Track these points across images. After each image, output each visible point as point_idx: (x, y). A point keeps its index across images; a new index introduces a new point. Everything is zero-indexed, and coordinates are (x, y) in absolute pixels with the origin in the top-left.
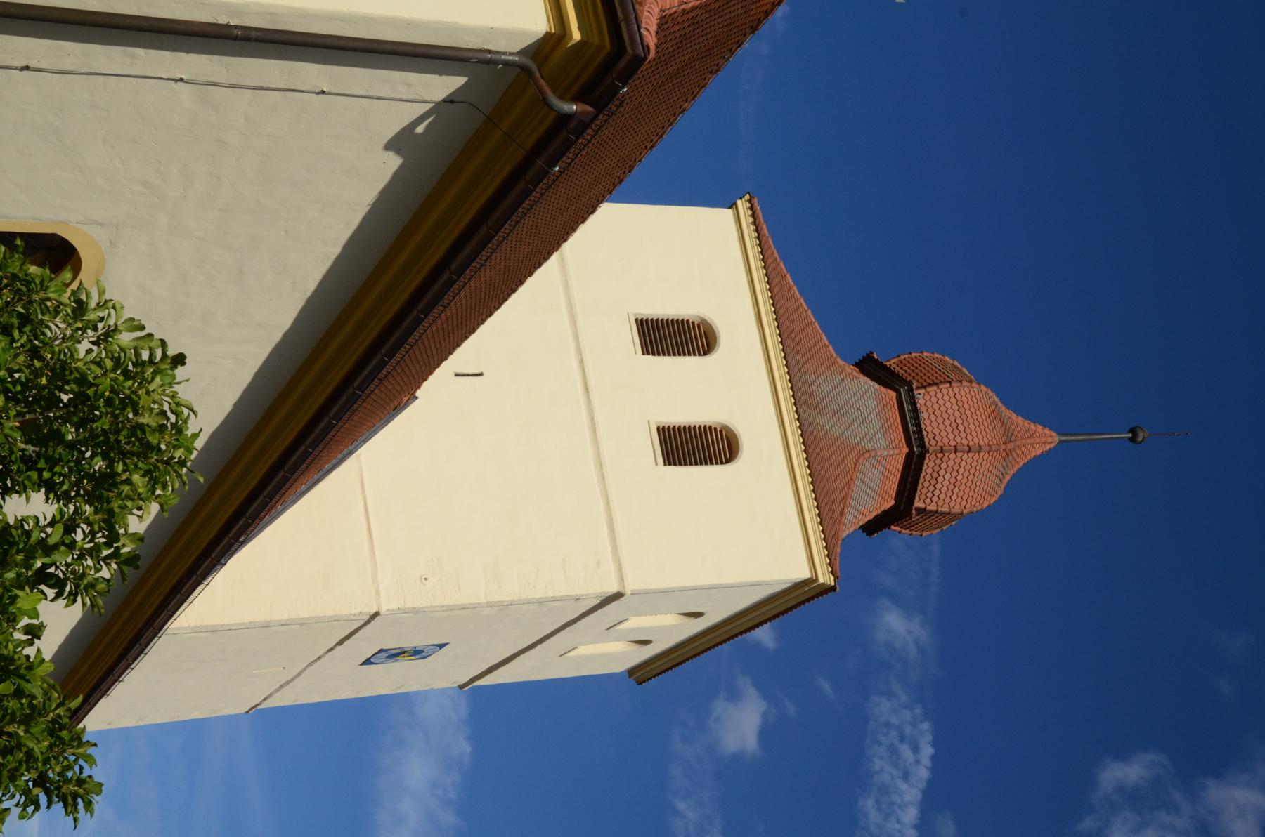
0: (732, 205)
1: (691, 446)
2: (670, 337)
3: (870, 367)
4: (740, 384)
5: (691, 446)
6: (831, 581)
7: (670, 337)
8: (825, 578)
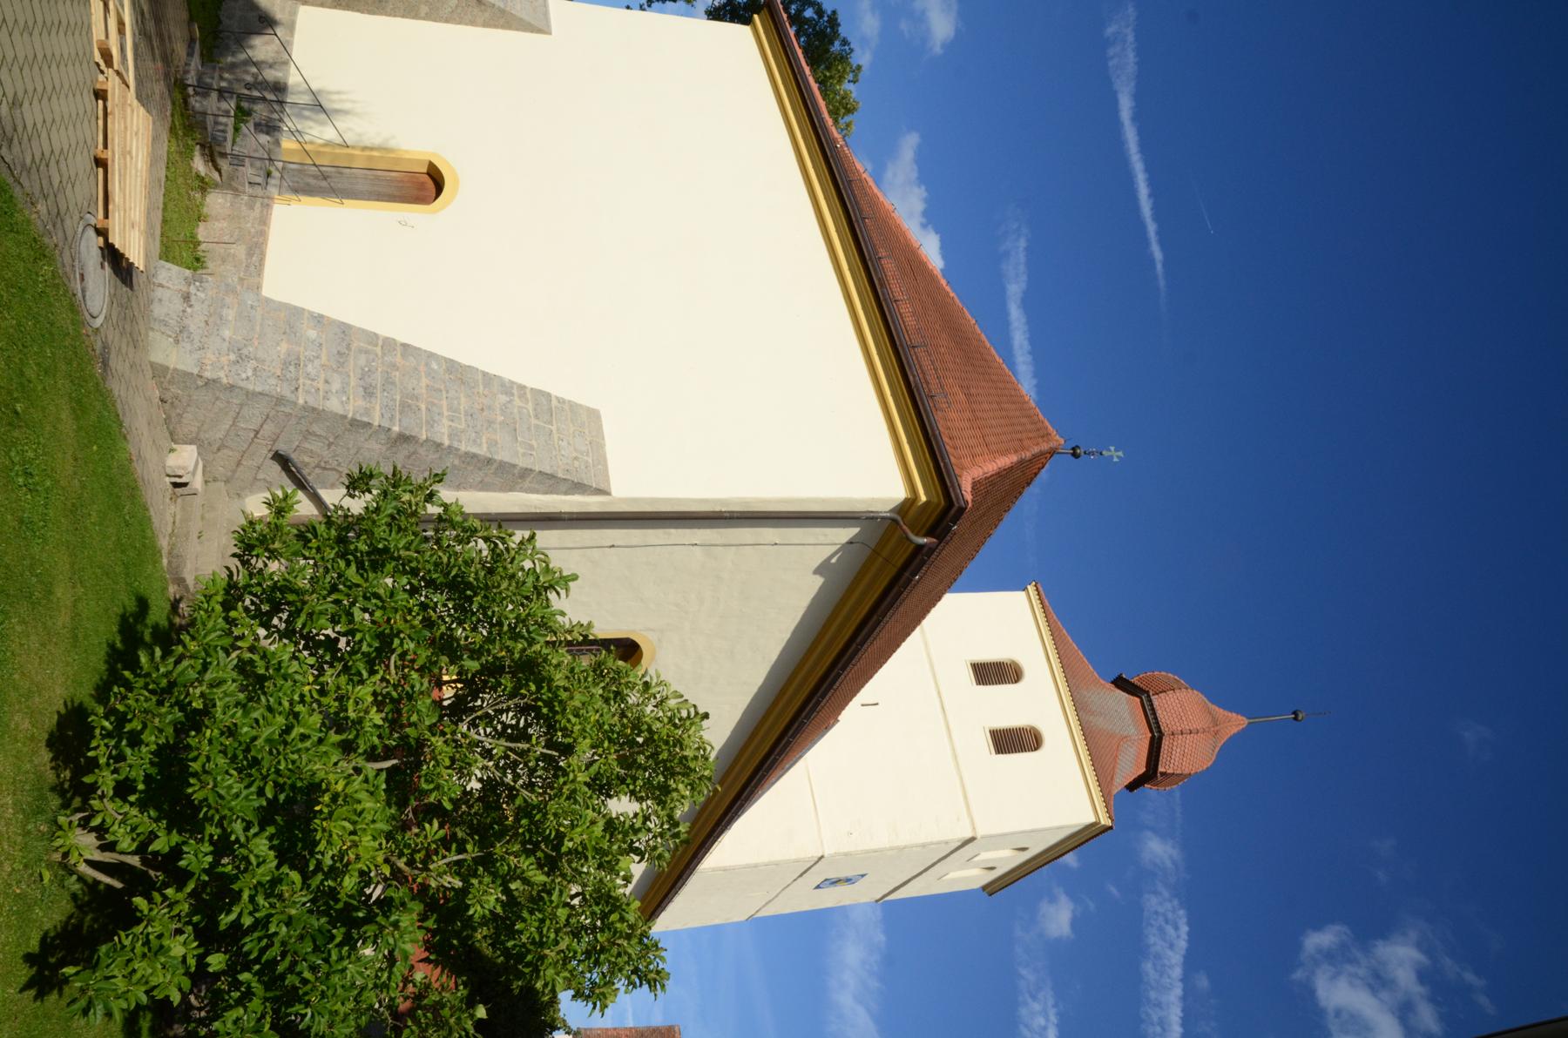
0: (1025, 589)
1: (1012, 741)
2: (992, 673)
3: (1121, 683)
4: (1039, 700)
5: (1012, 741)
6: (1109, 823)
7: (992, 673)
8: (1105, 821)
